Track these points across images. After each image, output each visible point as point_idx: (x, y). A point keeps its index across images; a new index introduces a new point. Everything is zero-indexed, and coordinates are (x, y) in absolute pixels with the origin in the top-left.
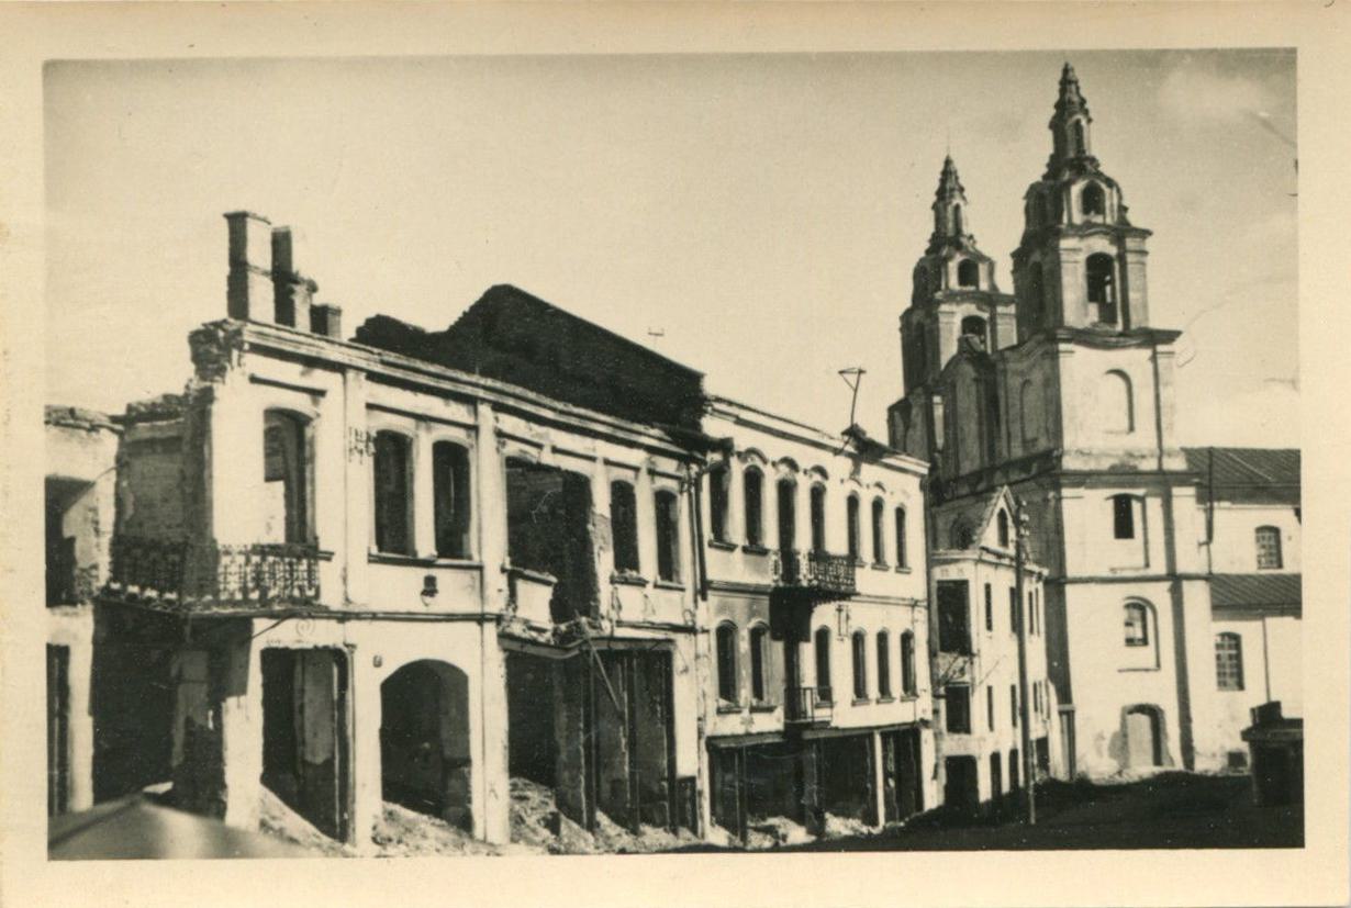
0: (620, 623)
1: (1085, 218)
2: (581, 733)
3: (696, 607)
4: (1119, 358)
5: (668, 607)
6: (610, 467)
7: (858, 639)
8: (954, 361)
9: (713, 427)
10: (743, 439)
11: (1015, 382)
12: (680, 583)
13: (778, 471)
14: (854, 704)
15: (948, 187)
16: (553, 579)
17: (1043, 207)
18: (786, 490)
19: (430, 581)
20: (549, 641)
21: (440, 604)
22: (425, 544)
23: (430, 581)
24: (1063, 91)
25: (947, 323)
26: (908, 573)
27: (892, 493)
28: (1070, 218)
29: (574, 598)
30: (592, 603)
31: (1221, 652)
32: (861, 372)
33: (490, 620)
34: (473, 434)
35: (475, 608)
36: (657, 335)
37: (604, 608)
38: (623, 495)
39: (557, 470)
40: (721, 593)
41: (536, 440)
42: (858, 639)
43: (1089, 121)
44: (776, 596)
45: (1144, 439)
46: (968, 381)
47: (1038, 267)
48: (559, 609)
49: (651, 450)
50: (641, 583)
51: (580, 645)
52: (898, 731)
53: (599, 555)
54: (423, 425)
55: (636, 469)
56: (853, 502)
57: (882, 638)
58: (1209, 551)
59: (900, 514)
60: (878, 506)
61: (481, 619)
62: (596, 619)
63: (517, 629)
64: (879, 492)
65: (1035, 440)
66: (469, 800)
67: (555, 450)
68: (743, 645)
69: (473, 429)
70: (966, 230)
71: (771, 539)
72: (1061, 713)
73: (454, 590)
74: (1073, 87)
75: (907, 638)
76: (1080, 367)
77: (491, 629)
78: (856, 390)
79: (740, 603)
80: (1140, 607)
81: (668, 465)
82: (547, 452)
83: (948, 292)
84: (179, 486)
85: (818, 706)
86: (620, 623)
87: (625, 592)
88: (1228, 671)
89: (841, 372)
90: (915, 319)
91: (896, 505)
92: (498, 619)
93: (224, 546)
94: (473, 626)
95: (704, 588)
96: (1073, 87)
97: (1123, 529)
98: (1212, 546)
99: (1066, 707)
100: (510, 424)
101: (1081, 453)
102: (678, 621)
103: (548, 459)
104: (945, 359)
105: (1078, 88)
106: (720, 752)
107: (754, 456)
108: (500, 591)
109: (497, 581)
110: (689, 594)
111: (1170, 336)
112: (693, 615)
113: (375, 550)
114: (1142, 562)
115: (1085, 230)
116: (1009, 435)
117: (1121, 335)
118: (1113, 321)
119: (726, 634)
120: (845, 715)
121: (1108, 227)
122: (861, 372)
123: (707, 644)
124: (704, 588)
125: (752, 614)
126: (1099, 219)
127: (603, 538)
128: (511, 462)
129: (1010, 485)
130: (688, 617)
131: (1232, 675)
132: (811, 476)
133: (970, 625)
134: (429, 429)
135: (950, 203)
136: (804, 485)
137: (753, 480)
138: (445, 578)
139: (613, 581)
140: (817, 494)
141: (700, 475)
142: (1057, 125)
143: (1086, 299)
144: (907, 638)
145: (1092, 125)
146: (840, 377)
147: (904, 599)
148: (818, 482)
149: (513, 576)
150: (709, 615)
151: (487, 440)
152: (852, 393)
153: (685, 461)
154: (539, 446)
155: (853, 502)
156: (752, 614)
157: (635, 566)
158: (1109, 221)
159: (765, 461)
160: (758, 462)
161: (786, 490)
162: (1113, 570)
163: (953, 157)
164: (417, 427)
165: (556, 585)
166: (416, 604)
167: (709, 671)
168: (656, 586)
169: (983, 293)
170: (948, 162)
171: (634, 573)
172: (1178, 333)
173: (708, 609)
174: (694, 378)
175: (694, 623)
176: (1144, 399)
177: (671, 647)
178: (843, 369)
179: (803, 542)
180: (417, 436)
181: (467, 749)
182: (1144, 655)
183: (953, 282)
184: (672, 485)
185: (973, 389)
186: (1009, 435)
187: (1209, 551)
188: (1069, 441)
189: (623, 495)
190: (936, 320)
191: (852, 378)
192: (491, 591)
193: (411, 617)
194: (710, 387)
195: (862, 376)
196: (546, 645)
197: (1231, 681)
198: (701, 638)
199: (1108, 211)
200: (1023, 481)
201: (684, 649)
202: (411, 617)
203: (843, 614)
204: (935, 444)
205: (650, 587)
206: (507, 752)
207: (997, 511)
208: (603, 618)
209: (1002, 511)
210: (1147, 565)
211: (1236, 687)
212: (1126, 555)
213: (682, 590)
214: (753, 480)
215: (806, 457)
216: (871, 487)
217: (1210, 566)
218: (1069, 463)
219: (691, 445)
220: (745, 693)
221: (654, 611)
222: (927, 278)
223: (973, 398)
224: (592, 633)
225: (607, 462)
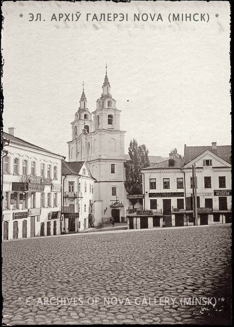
15: (83, 98)
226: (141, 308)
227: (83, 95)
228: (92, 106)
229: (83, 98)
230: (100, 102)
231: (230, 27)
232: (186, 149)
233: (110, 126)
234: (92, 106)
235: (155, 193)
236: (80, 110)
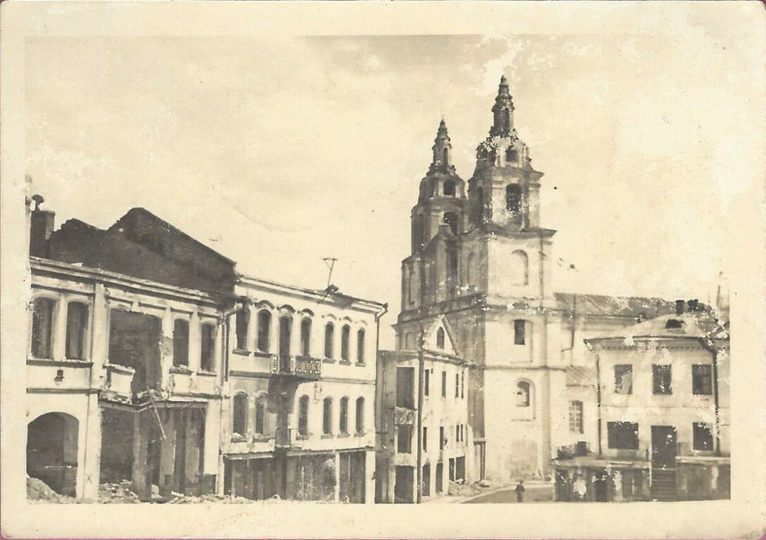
0: (173, 394)
2: (633, 486)
3: (222, 385)
4: (523, 245)
5: (206, 385)
6: (174, 313)
7: (328, 402)
8: (437, 238)
9: (239, 291)
10: (258, 296)
11: (465, 253)
12: (214, 372)
13: (281, 312)
14: (322, 437)
16: (134, 371)
17: (485, 156)
18: (286, 323)
19: (60, 372)
20: (129, 402)
21: (64, 385)
22: (59, 353)
23: (60, 372)
24: (500, 91)
25: (435, 216)
26: (364, 366)
27: (356, 323)
28: (499, 163)
29: (146, 377)
30: (158, 383)
31: (572, 412)
33: (94, 393)
34: (92, 298)
35: (86, 387)
36: (214, 241)
37: (164, 386)
38: (182, 328)
39: (140, 314)
40: (238, 377)
41: (129, 300)
42: (328, 402)
43: (513, 108)
44: (274, 379)
45: (532, 291)
46: (443, 249)
47: (480, 190)
48: (135, 387)
49: (200, 303)
50: (189, 373)
51: (148, 405)
53: (163, 358)
54: (62, 295)
55: (191, 313)
56: (330, 328)
57: (344, 401)
58: (572, 353)
59: (361, 333)
60: (346, 329)
61: (88, 392)
62: (159, 391)
63: (110, 397)
64: (347, 322)
66: (75, 484)
67: (140, 304)
68: (251, 406)
69: (93, 295)
70: (451, 163)
71: (274, 348)
72: (475, 443)
73: (74, 378)
74: (506, 90)
75: (360, 401)
76: (498, 249)
77: (94, 397)
78: (331, 269)
79: (251, 384)
80: (524, 385)
81: (212, 311)
82: (136, 304)
83: (437, 198)
85: (297, 439)
86: (173, 394)
87: (178, 378)
88: (576, 422)
89: (325, 259)
90: (419, 212)
91: (358, 329)
92: (99, 392)
94: (83, 397)
95: (227, 374)
96: (506, 90)
97: (519, 339)
98: (573, 350)
99: (481, 439)
100: (113, 292)
101: (498, 296)
102: (212, 392)
103: (135, 308)
104: (433, 236)
105: (508, 90)
106: (230, 463)
107: (265, 304)
108: (101, 377)
109: (99, 372)
110: (218, 379)
111: (552, 233)
112: (220, 390)
113: (31, 358)
114: (528, 359)
115: (506, 172)
117: (523, 231)
118: (520, 224)
119: (240, 400)
120: (316, 443)
121: (520, 169)
123: (228, 405)
124: (227, 374)
125: (259, 388)
126: (515, 165)
127: (168, 349)
128: (114, 311)
129: (446, 314)
130: (217, 389)
131: (577, 425)
132: (302, 314)
134: (66, 296)
135: (442, 147)
137: (265, 318)
138: (67, 371)
139: (171, 372)
140: (306, 325)
141: (228, 316)
142: (496, 110)
144: (360, 401)
145: (515, 111)
147: (359, 380)
148: (307, 318)
149: (110, 370)
150: (230, 388)
151: (100, 301)
152: (329, 271)
153: (220, 308)
154: (131, 303)
155: (330, 328)
156: (259, 388)
157: (186, 363)
158: (520, 166)
159: (273, 308)
160: (268, 308)
161: (286, 323)
163: (445, 121)
164: (59, 296)
165: (135, 374)
166: (52, 385)
167: (228, 420)
168: (198, 374)
169: (457, 199)
170: (442, 123)
171: (185, 367)
173: (230, 386)
174: (229, 264)
175: (221, 393)
176: (534, 268)
177: (206, 406)
179: (295, 349)
180: (59, 300)
181: (76, 458)
182: (527, 412)
183: (441, 192)
184: (214, 321)
185: (445, 256)
187: (572, 353)
188: (492, 288)
189: (182, 328)
190: (429, 214)
191: (330, 262)
192: (96, 377)
193: (47, 391)
194: (238, 269)
195: (335, 261)
196: (127, 405)
197: (577, 428)
198: (224, 401)
199: (520, 159)
201: (213, 406)
202: (47, 391)
203: (318, 389)
204: (425, 284)
205: (194, 375)
206: (99, 460)
207: (437, 329)
208: (163, 391)
209: (441, 328)
210: (532, 361)
211: (579, 433)
212: (521, 353)
213: (216, 376)
214: (265, 318)
215: (298, 305)
216: (338, 318)
217: (494, 368)
218: (490, 300)
219: (225, 301)
220: (251, 429)
221: (196, 387)
222: (427, 186)
223: (445, 260)
224: (157, 399)
225: (172, 310)
234: (464, 163)
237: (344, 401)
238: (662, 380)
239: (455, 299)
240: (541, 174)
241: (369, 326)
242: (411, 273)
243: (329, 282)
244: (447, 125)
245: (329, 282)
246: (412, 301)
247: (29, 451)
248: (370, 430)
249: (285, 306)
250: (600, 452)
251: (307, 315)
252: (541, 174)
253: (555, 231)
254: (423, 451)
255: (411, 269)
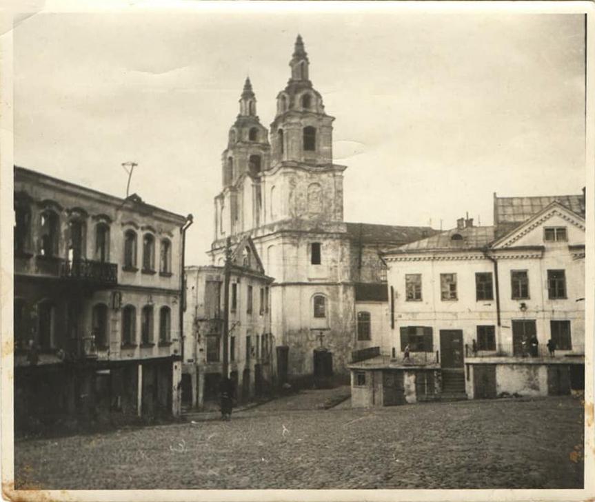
1: (304, 109)
15: (248, 94)
32: (134, 165)
52: (516, 227)
65: (276, 216)
84: (334, 241)
89: (123, 164)
93: (213, 251)
97: (316, 260)
116: (265, 212)
122: (134, 165)
133: (169, 329)
136: (140, 234)
143: (302, 148)
146: (122, 167)
152: (128, 176)
162: (310, 279)
172: (346, 167)
178: (124, 162)
186: (265, 212)
195: (135, 167)
200: (269, 235)
226: (241, 411)
227: (248, 86)
228: (267, 112)
229: (248, 94)
230: (284, 98)
231: (549, 341)
232: (500, 204)
233: (309, 156)
234: (267, 112)
235: (17, 231)
236: (241, 123)
237: (148, 310)
238: (450, 289)
239: (260, 226)
240: (334, 119)
241: (174, 238)
242: (222, 208)
243: (127, 193)
244: (252, 82)
245: (127, 193)
246: (223, 231)
247: (516, 345)
248: (175, 340)
249: (76, 209)
250: (394, 355)
251: (103, 221)
252: (334, 119)
253: (346, 167)
254: (249, 245)
255: (222, 203)
